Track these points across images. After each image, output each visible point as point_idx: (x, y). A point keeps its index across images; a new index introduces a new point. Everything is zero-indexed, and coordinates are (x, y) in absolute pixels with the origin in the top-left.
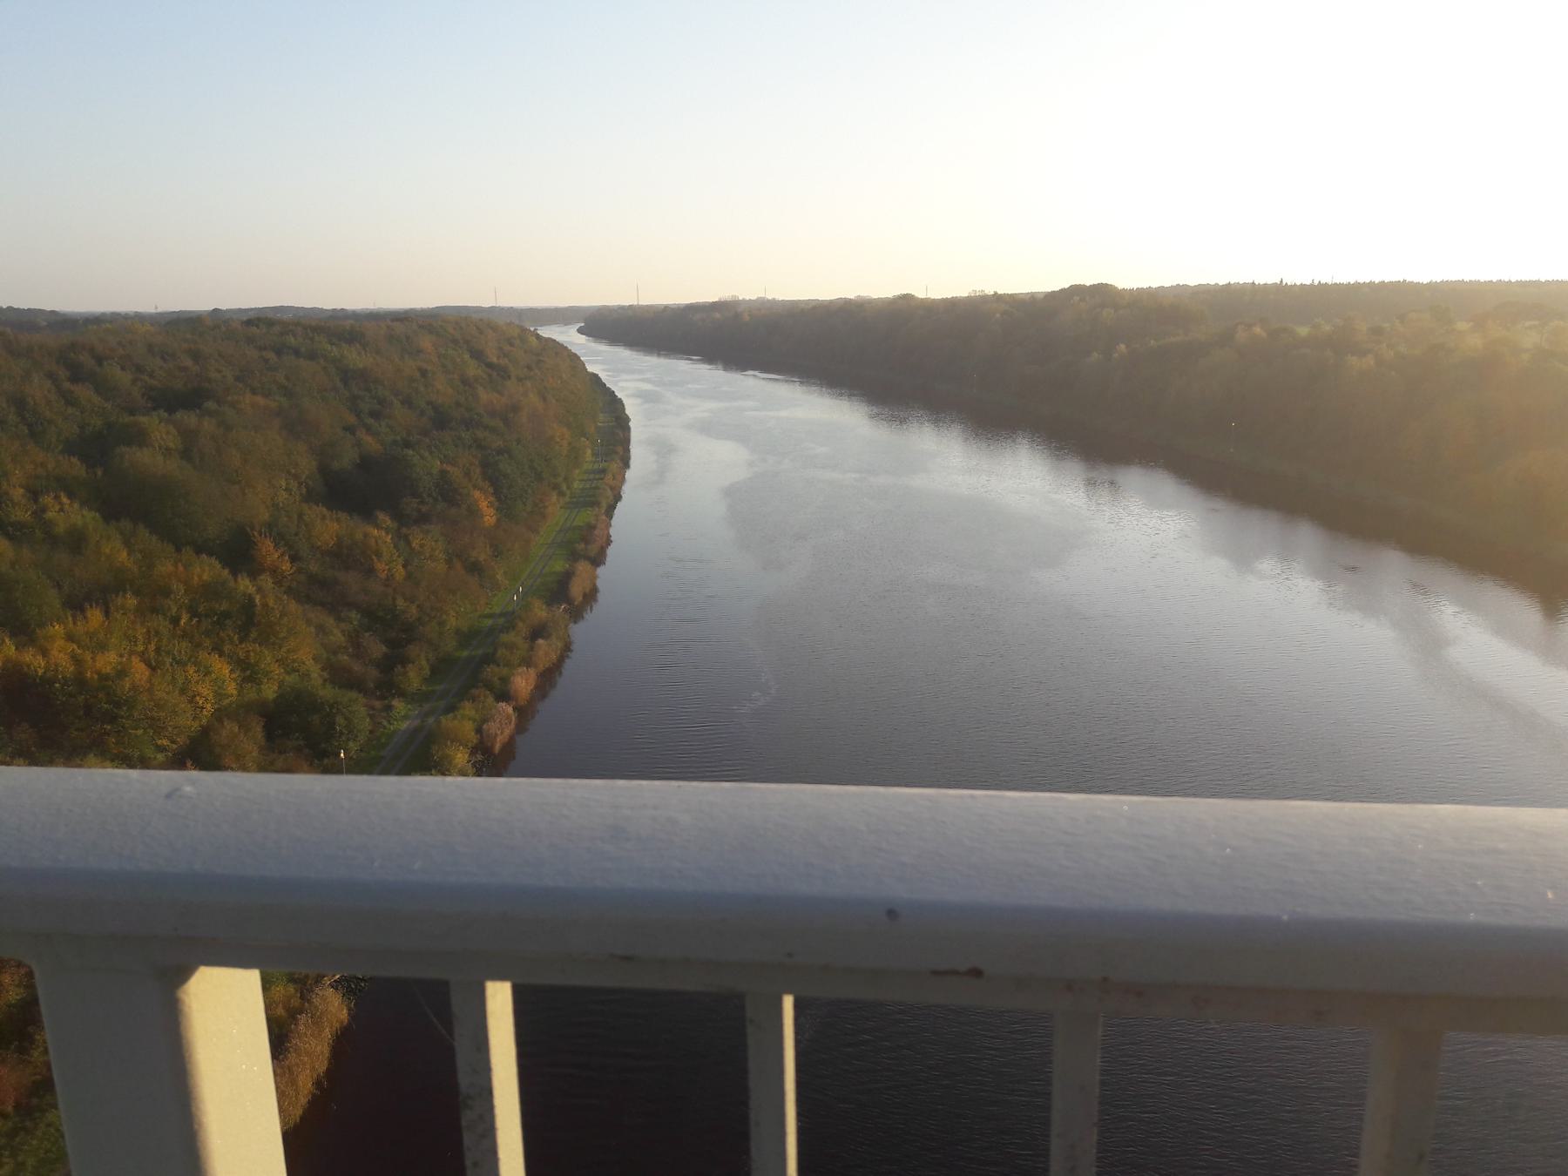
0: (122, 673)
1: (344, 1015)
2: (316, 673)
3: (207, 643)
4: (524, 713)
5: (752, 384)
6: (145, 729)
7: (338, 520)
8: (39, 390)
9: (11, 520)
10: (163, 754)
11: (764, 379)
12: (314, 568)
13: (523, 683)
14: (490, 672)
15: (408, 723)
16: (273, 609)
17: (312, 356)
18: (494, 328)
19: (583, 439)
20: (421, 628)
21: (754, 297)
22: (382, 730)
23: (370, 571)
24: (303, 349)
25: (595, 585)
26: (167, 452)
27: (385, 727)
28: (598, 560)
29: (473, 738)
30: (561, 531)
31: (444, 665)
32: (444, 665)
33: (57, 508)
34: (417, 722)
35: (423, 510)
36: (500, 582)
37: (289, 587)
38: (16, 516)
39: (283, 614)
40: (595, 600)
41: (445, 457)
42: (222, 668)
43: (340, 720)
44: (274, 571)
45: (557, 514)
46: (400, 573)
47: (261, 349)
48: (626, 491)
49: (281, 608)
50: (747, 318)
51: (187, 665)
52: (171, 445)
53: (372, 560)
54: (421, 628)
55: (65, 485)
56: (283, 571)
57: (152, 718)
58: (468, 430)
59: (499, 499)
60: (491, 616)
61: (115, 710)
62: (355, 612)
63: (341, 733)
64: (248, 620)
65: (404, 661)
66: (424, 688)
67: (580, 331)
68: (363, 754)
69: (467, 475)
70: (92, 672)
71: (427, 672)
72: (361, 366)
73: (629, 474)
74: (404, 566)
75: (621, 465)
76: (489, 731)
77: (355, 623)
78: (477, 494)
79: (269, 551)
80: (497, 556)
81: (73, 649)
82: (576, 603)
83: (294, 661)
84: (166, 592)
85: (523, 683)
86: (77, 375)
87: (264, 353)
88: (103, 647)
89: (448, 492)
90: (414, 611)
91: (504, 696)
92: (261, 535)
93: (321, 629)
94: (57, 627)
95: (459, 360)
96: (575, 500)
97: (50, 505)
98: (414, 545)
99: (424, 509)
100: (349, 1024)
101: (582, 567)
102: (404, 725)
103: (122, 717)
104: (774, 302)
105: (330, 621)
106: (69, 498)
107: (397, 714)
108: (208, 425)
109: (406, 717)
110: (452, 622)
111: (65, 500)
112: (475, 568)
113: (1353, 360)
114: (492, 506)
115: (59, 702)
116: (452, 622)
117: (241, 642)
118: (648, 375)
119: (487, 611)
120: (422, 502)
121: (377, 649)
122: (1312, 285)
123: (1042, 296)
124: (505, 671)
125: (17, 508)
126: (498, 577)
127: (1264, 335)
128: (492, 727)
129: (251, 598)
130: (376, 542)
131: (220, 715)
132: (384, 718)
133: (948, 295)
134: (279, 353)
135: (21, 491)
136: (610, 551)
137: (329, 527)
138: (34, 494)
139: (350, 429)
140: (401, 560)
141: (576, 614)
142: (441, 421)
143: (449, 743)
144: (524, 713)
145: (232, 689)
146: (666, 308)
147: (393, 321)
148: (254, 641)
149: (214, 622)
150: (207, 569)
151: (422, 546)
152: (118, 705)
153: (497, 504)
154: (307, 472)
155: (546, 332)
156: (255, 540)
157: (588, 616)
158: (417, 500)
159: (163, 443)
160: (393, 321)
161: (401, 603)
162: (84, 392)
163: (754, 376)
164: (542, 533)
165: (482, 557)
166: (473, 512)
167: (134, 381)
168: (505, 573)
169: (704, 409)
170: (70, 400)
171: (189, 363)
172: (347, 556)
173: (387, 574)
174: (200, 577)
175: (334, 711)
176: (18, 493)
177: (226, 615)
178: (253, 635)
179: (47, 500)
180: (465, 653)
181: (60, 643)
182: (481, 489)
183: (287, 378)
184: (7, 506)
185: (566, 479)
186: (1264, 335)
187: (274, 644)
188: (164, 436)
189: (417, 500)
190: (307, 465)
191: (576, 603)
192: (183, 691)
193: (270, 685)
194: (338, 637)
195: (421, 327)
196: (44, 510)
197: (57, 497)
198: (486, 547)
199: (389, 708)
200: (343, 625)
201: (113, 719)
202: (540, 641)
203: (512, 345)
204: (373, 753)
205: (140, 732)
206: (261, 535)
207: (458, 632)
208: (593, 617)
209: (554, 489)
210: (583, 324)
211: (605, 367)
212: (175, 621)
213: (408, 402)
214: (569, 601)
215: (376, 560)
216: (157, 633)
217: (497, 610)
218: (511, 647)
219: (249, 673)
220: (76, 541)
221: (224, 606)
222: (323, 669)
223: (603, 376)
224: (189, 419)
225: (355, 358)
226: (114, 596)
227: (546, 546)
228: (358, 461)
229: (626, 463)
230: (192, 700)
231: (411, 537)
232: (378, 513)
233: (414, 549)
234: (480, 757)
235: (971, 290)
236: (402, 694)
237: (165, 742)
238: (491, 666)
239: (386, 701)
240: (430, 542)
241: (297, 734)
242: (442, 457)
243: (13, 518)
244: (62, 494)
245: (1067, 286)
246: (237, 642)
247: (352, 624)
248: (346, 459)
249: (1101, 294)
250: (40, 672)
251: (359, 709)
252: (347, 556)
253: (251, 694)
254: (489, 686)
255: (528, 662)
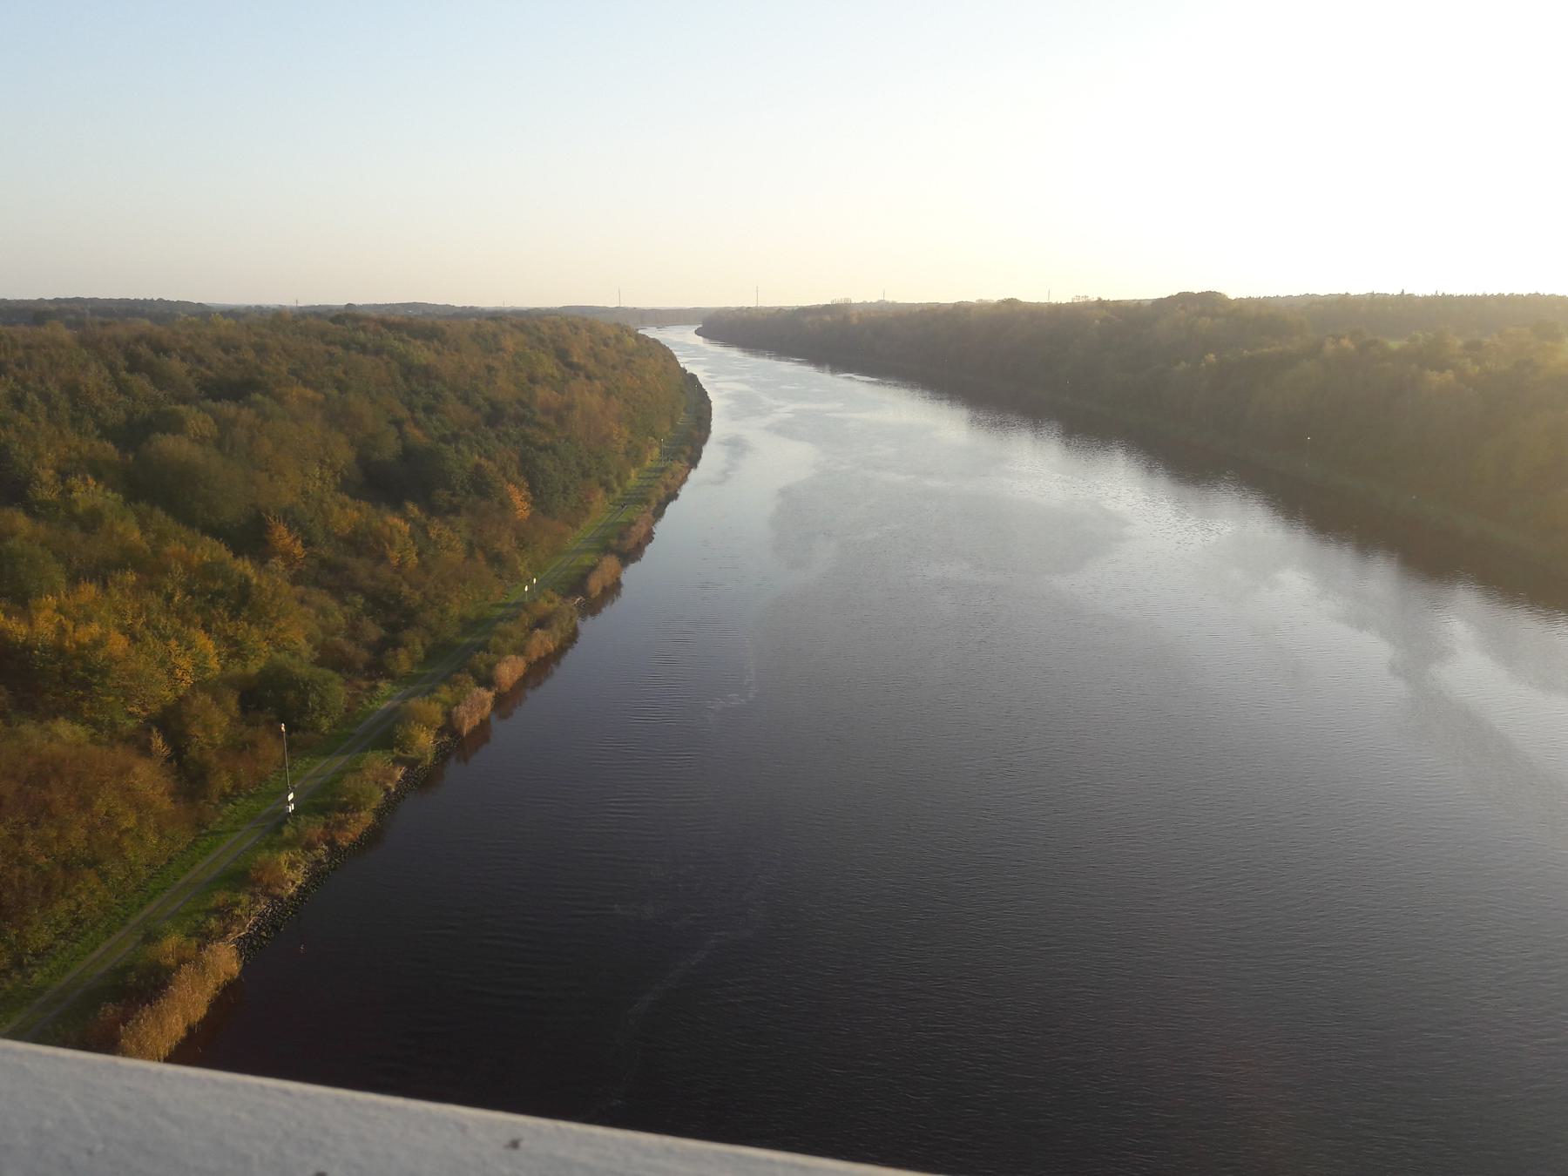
0: (98, 644)
1: (235, 968)
2: (306, 650)
3: (198, 619)
4: (504, 703)
5: (856, 387)
6: (117, 697)
7: (359, 509)
8: (94, 378)
9: (38, 499)
10: (135, 721)
11: (867, 382)
12: (326, 552)
13: (509, 670)
14: (480, 659)
15: (388, 703)
16: (266, 590)
17: (378, 352)
18: (591, 328)
19: (650, 438)
20: (421, 614)
21: (874, 300)
22: (360, 708)
23: (383, 558)
24: (370, 345)
25: (618, 579)
26: (201, 440)
27: (364, 706)
28: (630, 555)
29: (439, 719)
30: (602, 526)
31: (439, 651)
32: (439, 651)
33: (83, 489)
34: (396, 703)
35: (455, 502)
36: (522, 573)
37: (299, 570)
38: (43, 495)
39: (275, 595)
40: (618, 594)
41: (485, 451)
42: (206, 644)
43: (313, 697)
44: (287, 555)
45: (601, 509)
46: (413, 560)
47: (329, 343)
48: (685, 492)
49: (273, 590)
50: (855, 321)
51: (170, 639)
52: (206, 433)
53: (385, 547)
54: (421, 614)
55: (97, 470)
56: (295, 555)
57: (125, 687)
58: (517, 426)
59: (534, 495)
60: (505, 605)
61: (89, 678)
62: (360, 596)
63: (314, 710)
64: (242, 600)
65: (396, 644)
66: (415, 671)
67: (698, 332)
68: (335, 731)
69: (503, 469)
70: (70, 642)
71: (421, 655)
72: (424, 362)
73: (694, 475)
74: (419, 555)
75: (687, 464)
76: (457, 714)
77: (359, 606)
78: (511, 488)
79: (282, 536)
80: (522, 549)
81: (60, 620)
82: (593, 596)
83: (283, 640)
84: (165, 570)
85: (509, 670)
86: (135, 365)
87: (332, 349)
88: (89, 619)
89: (480, 485)
90: (418, 598)
91: (487, 682)
92: (275, 520)
93: (323, 611)
94: (50, 599)
95: (534, 358)
96: (628, 497)
97: (77, 486)
98: (431, 535)
99: (456, 500)
100: (239, 979)
101: (611, 562)
102: (384, 706)
103: (95, 684)
104: (894, 304)
105: (332, 604)
106: (95, 480)
107: (380, 695)
108: (247, 415)
109: (389, 698)
110: (455, 610)
111: (91, 481)
112: (496, 559)
113: (1434, 377)
114: (526, 500)
115: (36, 668)
116: (455, 610)
117: (230, 620)
118: (748, 376)
119: (503, 600)
120: (453, 495)
121: (373, 631)
122: (1436, 297)
123: (1150, 303)
124: (493, 657)
125: (44, 487)
126: (521, 568)
127: (1352, 347)
128: (461, 711)
129: (247, 580)
130: (391, 531)
131: (201, 685)
132: (367, 697)
133: (18, 297)
134: (346, 347)
135: (51, 472)
136: (649, 549)
137: (349, 515)
138: (63, 475)
139: (398, 423)
140: (415, 549)
141: (592, 607)
142: (495, 416)
143: (413, 722)
144: (504, 703)
145: (214, 664)
146: (780, 310)
147: (487, 319)
148: (245, 620)
149: (207, 600)
150: (210, 550)
151: (439, 536)
152: (92, 672)
153: (531, 498)
154: (343, 462)
155: (651, 333)
156: (270, 524)
157: (607, 611)
158: (450, 492)
159: (198, 431)
160: (487, 319)
161: (405, 589)
162: (141, 382)
163: (850, 378)
164: (582, 528)
165: (506, 548)
166: (505, 505)
167: (189, 373)
168: (530, 565)
169: (785, 411)
170: (123, 388)
171: (250, 355)
172: (363, 543)
173: (399, 562)
174: (201, 558)
175: (309, 688)
176: (47, 475)
177: (221, 594)
178: (245, 613)
179: (74, 481)
180: (467, 640)
181: (48, 612)
182: (516, 484)
183: (345, 373)
184: (35, 485)
185: (618, 477)
186: (1352, 347)
187: (265, 623)
188: (200, 424)
189: (450, 492)
190: (344, 455)
191: (593, 596)
192: (162, 663)
193: (256, 661)
194: (338, 617)
195: (514, 326)
196: (70, 492)
197: (85, 480)
198: (511, 538)
199: (375, 688)
200: (346, 609)
201: (86, 685)
202: (538, 631)
203: (606, 345)
204: (345, 730)
205: (111, 699)
206: (275, 520)
207: (463, 619)
208: (611, 612)
209: (601, 485)
210: (701, 326)
211: (707, 367)
212: (169, 598)
213: (465, 400)
214: (586, 594)
215: (388, 547)
216: (148, 608)
217: (512, 600)
218: (505, 635)
219: (235, 649)
220: (91, 522)
221: (219, 585)
222: (315, 649)
223: (701, 378)
224: (229, 409)
225: (422, 354)
226: (114, 572)
227: (582, 541)
228: (401, 453)
229: (694, 461)
230: (171, 673)
231: (429, 528)
232: (407, 504)
233: (431, 539)
234: (447, 738)
235: (1074, 296)
236: (390, 676)
237: (135, 709)
238: (481, 652)
239: (373, 682)
240: (451, 537)
241: (269, 708)
242: (482, 451)
243: (40, 497)
244: (89, 477)
245: (1175, 293)
246: (227, 620)
247: (355, 607)
248: (389, 448)
249: (1210, 301)
250: (21, 639)
251: (339, 691)
252: (363, 543)
253: (236, 669)
254: (475, 673)
255: (519, 650)
